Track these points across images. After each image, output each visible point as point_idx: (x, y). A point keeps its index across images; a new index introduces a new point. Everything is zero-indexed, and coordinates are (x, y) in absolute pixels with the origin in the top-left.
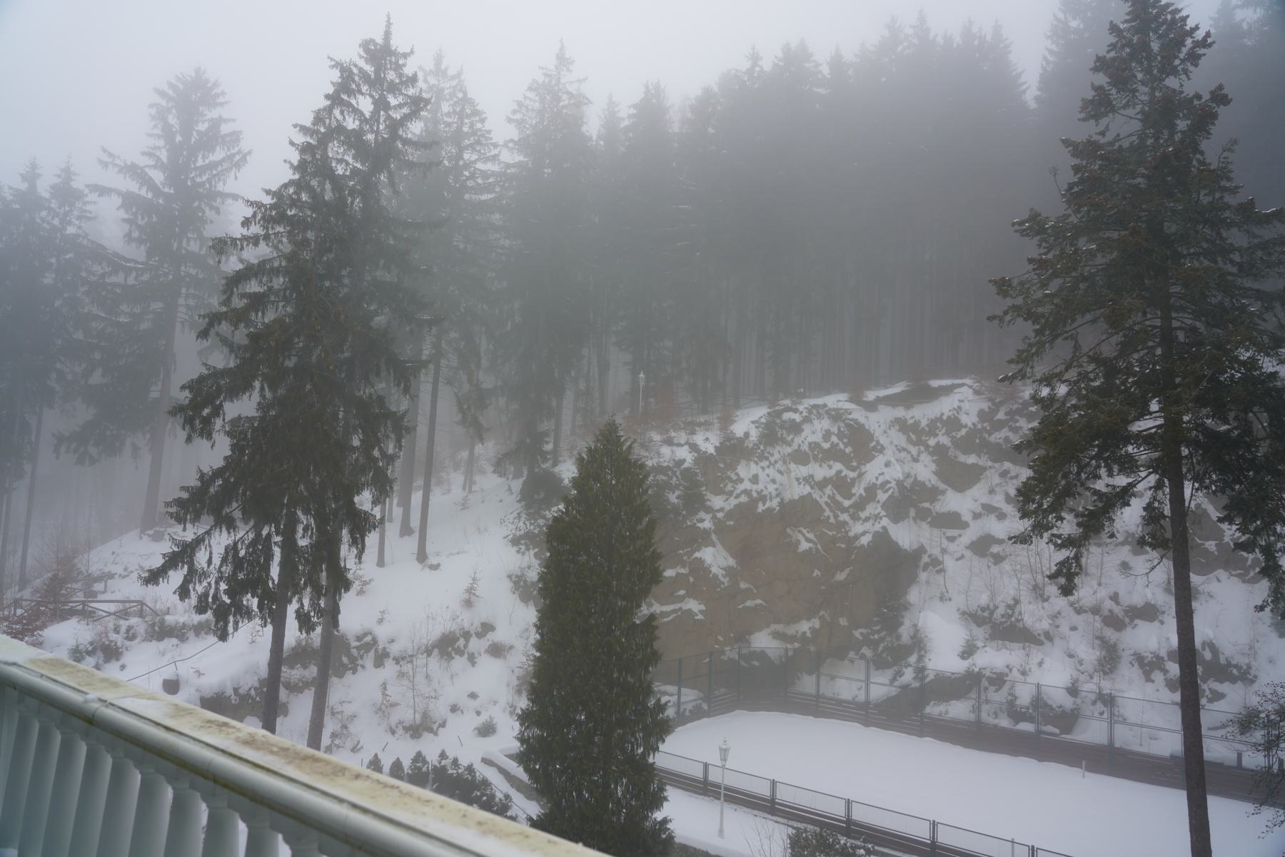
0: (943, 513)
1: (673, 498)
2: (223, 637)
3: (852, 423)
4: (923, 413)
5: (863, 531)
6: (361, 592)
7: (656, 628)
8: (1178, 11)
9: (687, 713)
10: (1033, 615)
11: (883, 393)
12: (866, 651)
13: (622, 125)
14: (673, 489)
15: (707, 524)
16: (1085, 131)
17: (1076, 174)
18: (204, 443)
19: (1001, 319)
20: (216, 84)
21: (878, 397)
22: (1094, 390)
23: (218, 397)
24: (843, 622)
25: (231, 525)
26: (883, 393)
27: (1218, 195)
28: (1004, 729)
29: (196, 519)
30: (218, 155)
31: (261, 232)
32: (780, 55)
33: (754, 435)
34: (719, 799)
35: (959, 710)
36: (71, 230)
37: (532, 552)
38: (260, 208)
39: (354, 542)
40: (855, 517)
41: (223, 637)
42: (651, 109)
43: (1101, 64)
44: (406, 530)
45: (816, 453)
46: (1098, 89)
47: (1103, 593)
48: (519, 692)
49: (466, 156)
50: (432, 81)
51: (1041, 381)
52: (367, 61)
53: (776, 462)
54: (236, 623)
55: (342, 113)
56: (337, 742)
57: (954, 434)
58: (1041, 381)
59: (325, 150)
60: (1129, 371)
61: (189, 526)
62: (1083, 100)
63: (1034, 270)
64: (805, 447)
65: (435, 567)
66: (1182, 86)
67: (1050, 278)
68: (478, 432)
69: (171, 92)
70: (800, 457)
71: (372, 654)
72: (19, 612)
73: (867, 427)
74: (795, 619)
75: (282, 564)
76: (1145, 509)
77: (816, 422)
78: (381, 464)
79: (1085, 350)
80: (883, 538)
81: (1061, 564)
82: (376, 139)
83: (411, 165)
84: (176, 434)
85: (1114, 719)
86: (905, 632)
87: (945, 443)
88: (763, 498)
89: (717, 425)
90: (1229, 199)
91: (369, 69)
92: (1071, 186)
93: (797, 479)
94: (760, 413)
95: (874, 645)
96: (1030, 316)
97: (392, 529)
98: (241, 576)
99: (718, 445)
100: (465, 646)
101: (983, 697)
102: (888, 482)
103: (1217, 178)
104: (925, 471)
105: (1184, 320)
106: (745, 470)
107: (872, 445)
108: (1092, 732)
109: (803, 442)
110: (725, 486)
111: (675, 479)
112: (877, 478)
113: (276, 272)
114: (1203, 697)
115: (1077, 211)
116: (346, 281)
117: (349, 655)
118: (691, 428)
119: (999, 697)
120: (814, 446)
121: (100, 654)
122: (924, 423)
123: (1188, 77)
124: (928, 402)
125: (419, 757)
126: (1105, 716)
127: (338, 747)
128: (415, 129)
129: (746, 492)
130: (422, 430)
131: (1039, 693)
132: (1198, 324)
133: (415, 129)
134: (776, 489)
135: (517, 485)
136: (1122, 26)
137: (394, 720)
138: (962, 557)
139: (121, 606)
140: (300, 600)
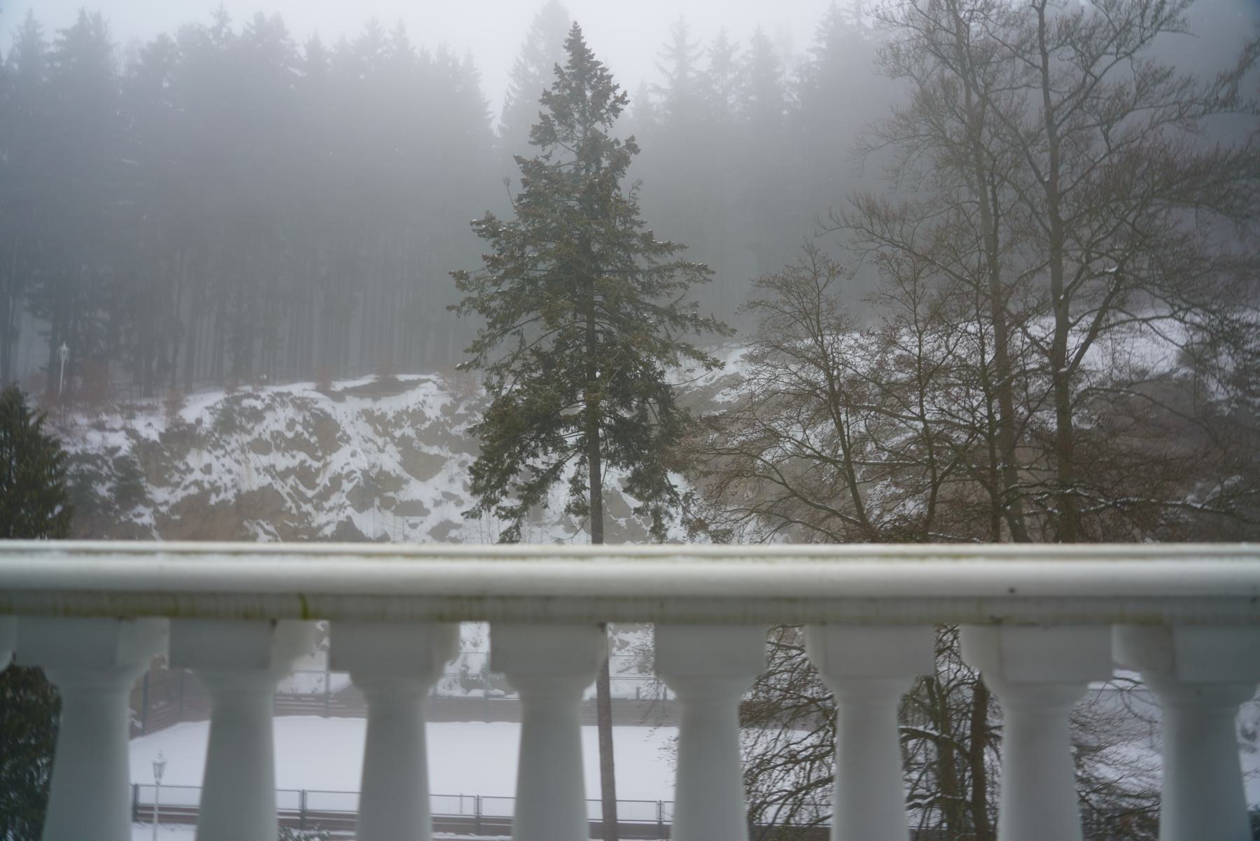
0: (407, 502)
1: (103, 490)
3: (318, 412)
4: (389, 406)
8: (604, 70)
11: (351, 384)
13: (47, 51)
14: (102, 480)
16: (534, 153)
17: (525, 187)
19: (459, 310)
21: (345, 388)
22: (534, 381)
26: (351, 384)
27: (628, 225)
32: (252, 22)
40: (318, 508)
43: (547, 99)
45: (278, 442)
46: (544, 117)
51: (492, 370)
53: (233, 451)
57: (418, 426)
58: (492, 370)
62: (533, 126)
63: (488, 266)
64: (267, 436)
66: (606, 131)
67: (502, 278)
70: (261, 447)
73: (334, 417)
77: (279, 410)
87: (410, 435)
88: (216, 489)
89: (162, 409)
90: (636, 229)
92: (520, 198)
93: (257, 470)
94: (216, 398)
96: (484, 310)
99: (163, 430)
102: (353, 472)
103: (628, 211)
104: (390, 461)
105: (604, 325)
106: (195, 460)
107: (338, 435)
109: (264, 431)
110: (171, 476)
111: (105, 469)
112: (342, 468)
114: (614, 646)
118: (130, 412)
120: (277, 435)
122: (390, 415)
123: (611, 124)
124: (394, 395)
129: (198, 483)
132: (613, 329)
134: (232, 480)
136: (565, 71)
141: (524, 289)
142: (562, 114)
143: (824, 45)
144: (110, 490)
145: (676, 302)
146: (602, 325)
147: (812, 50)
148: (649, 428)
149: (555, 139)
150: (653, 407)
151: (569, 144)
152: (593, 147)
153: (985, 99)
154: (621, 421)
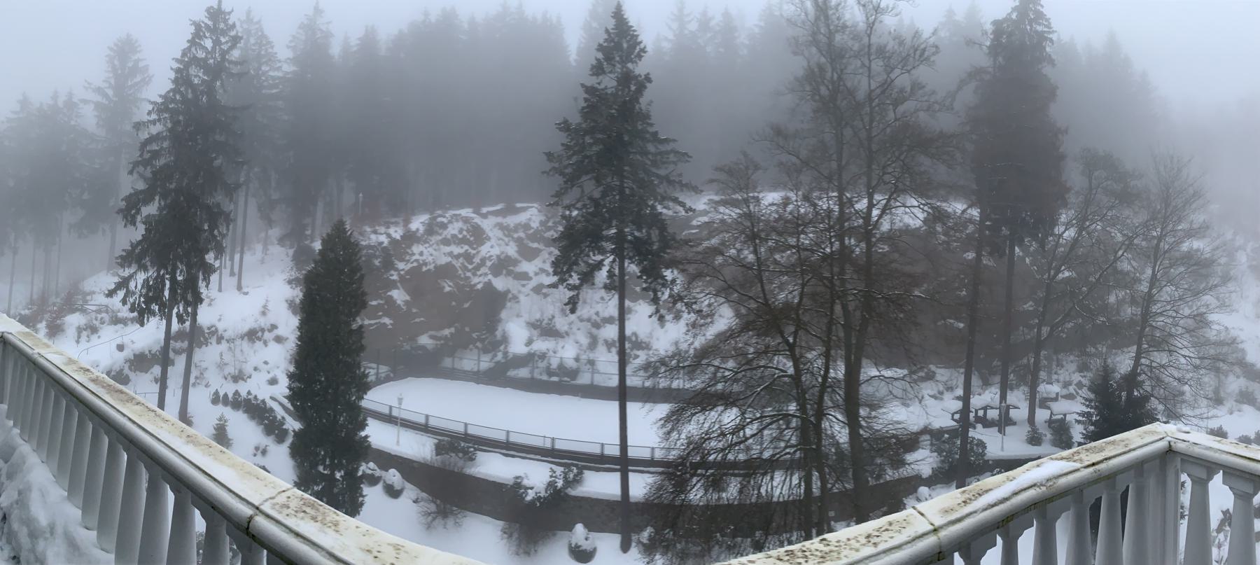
1: (377, 262)
2: (142, 325)
4: (512, 220)
5: (478, 281)
6: (210, 305)
7: (363, 332)
8: (635, 31)
9: (382, 379)
10: (561, 323)
12: (479, 344)
15: (395, 277)
16: (592, 81)
17: (586, 102)
18: (133, 228)
20: (136, 41)
23: (139, 204)
24: (467, 329)
25: (146, 270)
28: (544, 381)
29: (129, 266)
30: (138, 79)
31: (156, 117)
33: (422, 229)
34: (397, 425)
35: (523, 373)
36: (73, 123)
37: (299, 288)
38: (155, 105)
39: (204, 279)
40: (475, 275)
41: (142, 325)
42: (369, 40)
43: (600, 48)
44: (232, 274)
47: (593, 311)
48: (291, 362)
49: (263, 68)
50: (245, 26)
52: (209, 20)
53: (433, 244)
54: (148, 318)
55: (196, 49)
56: (198, 381)
59: (188, 71)
60: (604, 206)
61: (126, 269)
64: (449, 237)
65: (246, 294)
67: (573, 155)
68: (270, 223)
69: (115, 48)
70: (446, 242)
71: (215, 337)
72: (55, 308)
74: (442, 328)
75: (170, 289)
76: (607, 272)
77: (455, 224)
78: (218, 238)
79: (586, 192)
80: (489, 285)
81: (570, 298)
82: (214, 62)
83: (232, 75)
84: (120, 223)
85: (594, 371)
86: (499, 334)
88: (425, 264)
89: (402, 224)
91: (210, 23)
93: (444, 254)
94: (425, 218)
95: (482, 341)
96: (562, 174)
97: (226, 272)
98: (151, 294)
100: (262, 336)
101: (535, 365)
102: (492, 256)
103: (645, 117)
104: (512, 250)
106: (416, 249)
108: (584, 379)
110: (406, 257)
113: (164, 138)
115: (585, 122)
116: (200, 141)
117: (204, 337)
119: (542, 365)
120: (454, 236)
121: (89, 330)
122: (512, 225)
125: (236, 393)
126: (590, 370)
127: (198, 384)
128: (236, 54)
129: (417, 261)
130: (240, 221)
131: (561, 361)
132: (634, 187)
133: (236, 54)
134: (433, 259)
135: (291, 252)
136: (611, 31)
137: (226, 373)
138: (528, 295)
139: (98, 307)
140: (178, 308)
141: (583, 161)
142: (609, 59)
143: (762, 24)
144: (379, 262)
145: (670, 173)
146: (628, 183)
147: (756, 25)
148: (653, 243)
149: (604, 72)
150: (655, 234)
151: (612, 76)
152: (626, 78)
153: (840, 78)
154: (636, 237)
